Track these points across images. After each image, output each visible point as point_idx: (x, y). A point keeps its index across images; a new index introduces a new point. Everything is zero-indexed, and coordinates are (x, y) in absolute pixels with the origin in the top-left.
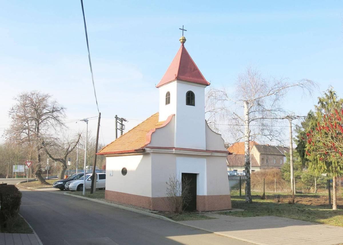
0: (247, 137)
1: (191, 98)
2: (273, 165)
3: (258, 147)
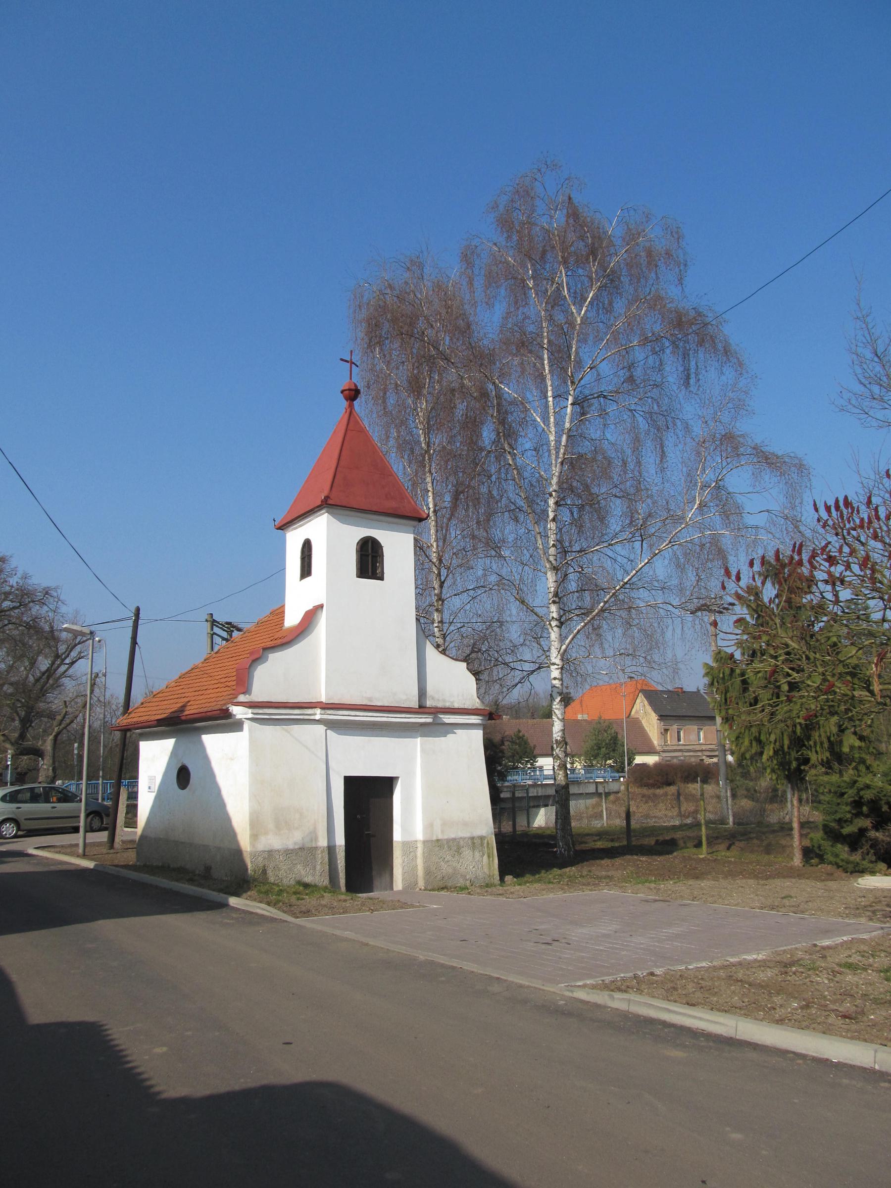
0: (556, 667)
1: (373, 557)
2: (698, 748)
3: (653, 697)
